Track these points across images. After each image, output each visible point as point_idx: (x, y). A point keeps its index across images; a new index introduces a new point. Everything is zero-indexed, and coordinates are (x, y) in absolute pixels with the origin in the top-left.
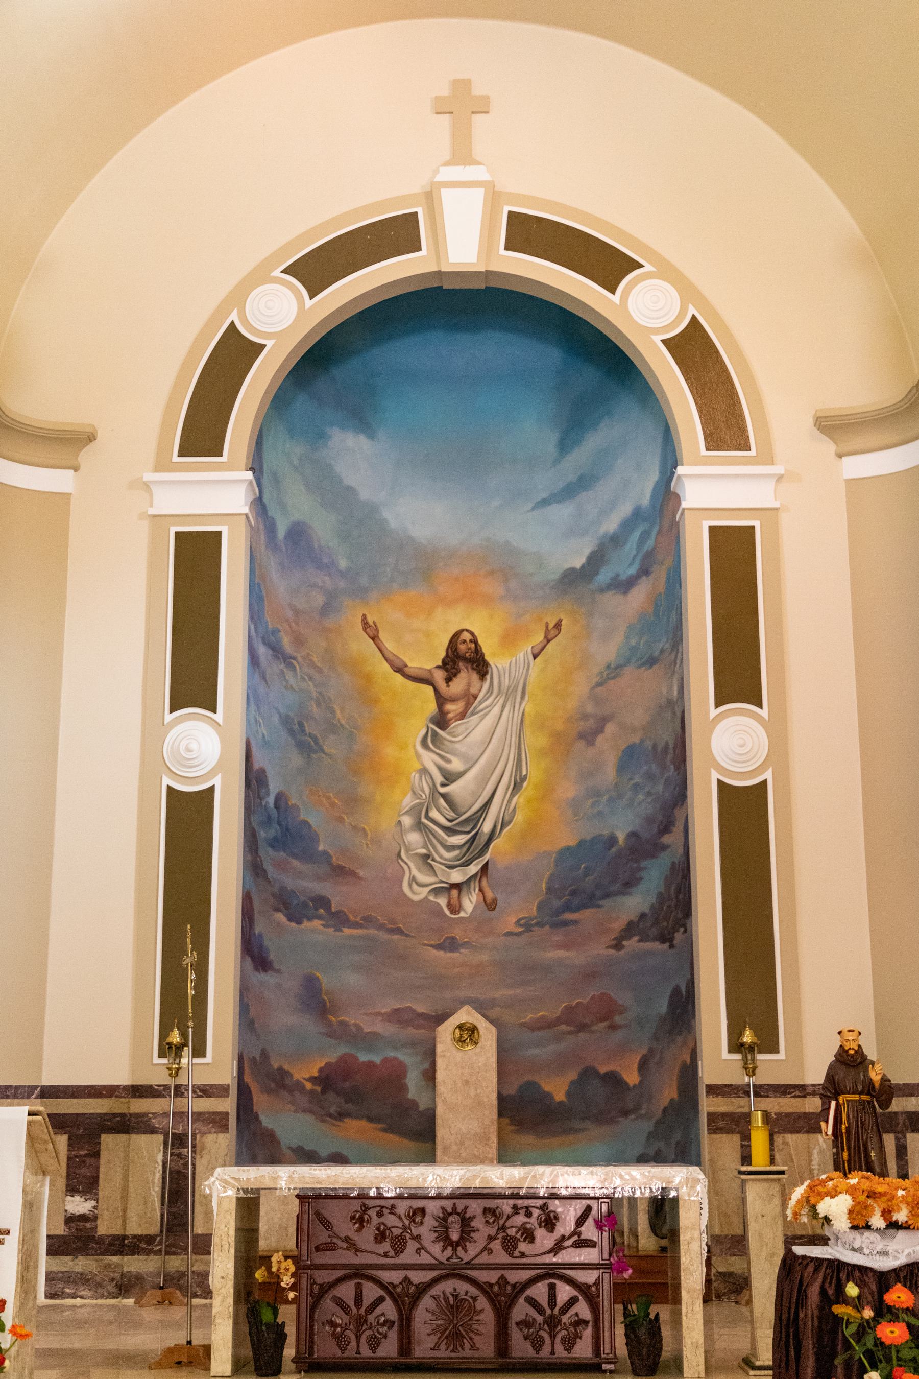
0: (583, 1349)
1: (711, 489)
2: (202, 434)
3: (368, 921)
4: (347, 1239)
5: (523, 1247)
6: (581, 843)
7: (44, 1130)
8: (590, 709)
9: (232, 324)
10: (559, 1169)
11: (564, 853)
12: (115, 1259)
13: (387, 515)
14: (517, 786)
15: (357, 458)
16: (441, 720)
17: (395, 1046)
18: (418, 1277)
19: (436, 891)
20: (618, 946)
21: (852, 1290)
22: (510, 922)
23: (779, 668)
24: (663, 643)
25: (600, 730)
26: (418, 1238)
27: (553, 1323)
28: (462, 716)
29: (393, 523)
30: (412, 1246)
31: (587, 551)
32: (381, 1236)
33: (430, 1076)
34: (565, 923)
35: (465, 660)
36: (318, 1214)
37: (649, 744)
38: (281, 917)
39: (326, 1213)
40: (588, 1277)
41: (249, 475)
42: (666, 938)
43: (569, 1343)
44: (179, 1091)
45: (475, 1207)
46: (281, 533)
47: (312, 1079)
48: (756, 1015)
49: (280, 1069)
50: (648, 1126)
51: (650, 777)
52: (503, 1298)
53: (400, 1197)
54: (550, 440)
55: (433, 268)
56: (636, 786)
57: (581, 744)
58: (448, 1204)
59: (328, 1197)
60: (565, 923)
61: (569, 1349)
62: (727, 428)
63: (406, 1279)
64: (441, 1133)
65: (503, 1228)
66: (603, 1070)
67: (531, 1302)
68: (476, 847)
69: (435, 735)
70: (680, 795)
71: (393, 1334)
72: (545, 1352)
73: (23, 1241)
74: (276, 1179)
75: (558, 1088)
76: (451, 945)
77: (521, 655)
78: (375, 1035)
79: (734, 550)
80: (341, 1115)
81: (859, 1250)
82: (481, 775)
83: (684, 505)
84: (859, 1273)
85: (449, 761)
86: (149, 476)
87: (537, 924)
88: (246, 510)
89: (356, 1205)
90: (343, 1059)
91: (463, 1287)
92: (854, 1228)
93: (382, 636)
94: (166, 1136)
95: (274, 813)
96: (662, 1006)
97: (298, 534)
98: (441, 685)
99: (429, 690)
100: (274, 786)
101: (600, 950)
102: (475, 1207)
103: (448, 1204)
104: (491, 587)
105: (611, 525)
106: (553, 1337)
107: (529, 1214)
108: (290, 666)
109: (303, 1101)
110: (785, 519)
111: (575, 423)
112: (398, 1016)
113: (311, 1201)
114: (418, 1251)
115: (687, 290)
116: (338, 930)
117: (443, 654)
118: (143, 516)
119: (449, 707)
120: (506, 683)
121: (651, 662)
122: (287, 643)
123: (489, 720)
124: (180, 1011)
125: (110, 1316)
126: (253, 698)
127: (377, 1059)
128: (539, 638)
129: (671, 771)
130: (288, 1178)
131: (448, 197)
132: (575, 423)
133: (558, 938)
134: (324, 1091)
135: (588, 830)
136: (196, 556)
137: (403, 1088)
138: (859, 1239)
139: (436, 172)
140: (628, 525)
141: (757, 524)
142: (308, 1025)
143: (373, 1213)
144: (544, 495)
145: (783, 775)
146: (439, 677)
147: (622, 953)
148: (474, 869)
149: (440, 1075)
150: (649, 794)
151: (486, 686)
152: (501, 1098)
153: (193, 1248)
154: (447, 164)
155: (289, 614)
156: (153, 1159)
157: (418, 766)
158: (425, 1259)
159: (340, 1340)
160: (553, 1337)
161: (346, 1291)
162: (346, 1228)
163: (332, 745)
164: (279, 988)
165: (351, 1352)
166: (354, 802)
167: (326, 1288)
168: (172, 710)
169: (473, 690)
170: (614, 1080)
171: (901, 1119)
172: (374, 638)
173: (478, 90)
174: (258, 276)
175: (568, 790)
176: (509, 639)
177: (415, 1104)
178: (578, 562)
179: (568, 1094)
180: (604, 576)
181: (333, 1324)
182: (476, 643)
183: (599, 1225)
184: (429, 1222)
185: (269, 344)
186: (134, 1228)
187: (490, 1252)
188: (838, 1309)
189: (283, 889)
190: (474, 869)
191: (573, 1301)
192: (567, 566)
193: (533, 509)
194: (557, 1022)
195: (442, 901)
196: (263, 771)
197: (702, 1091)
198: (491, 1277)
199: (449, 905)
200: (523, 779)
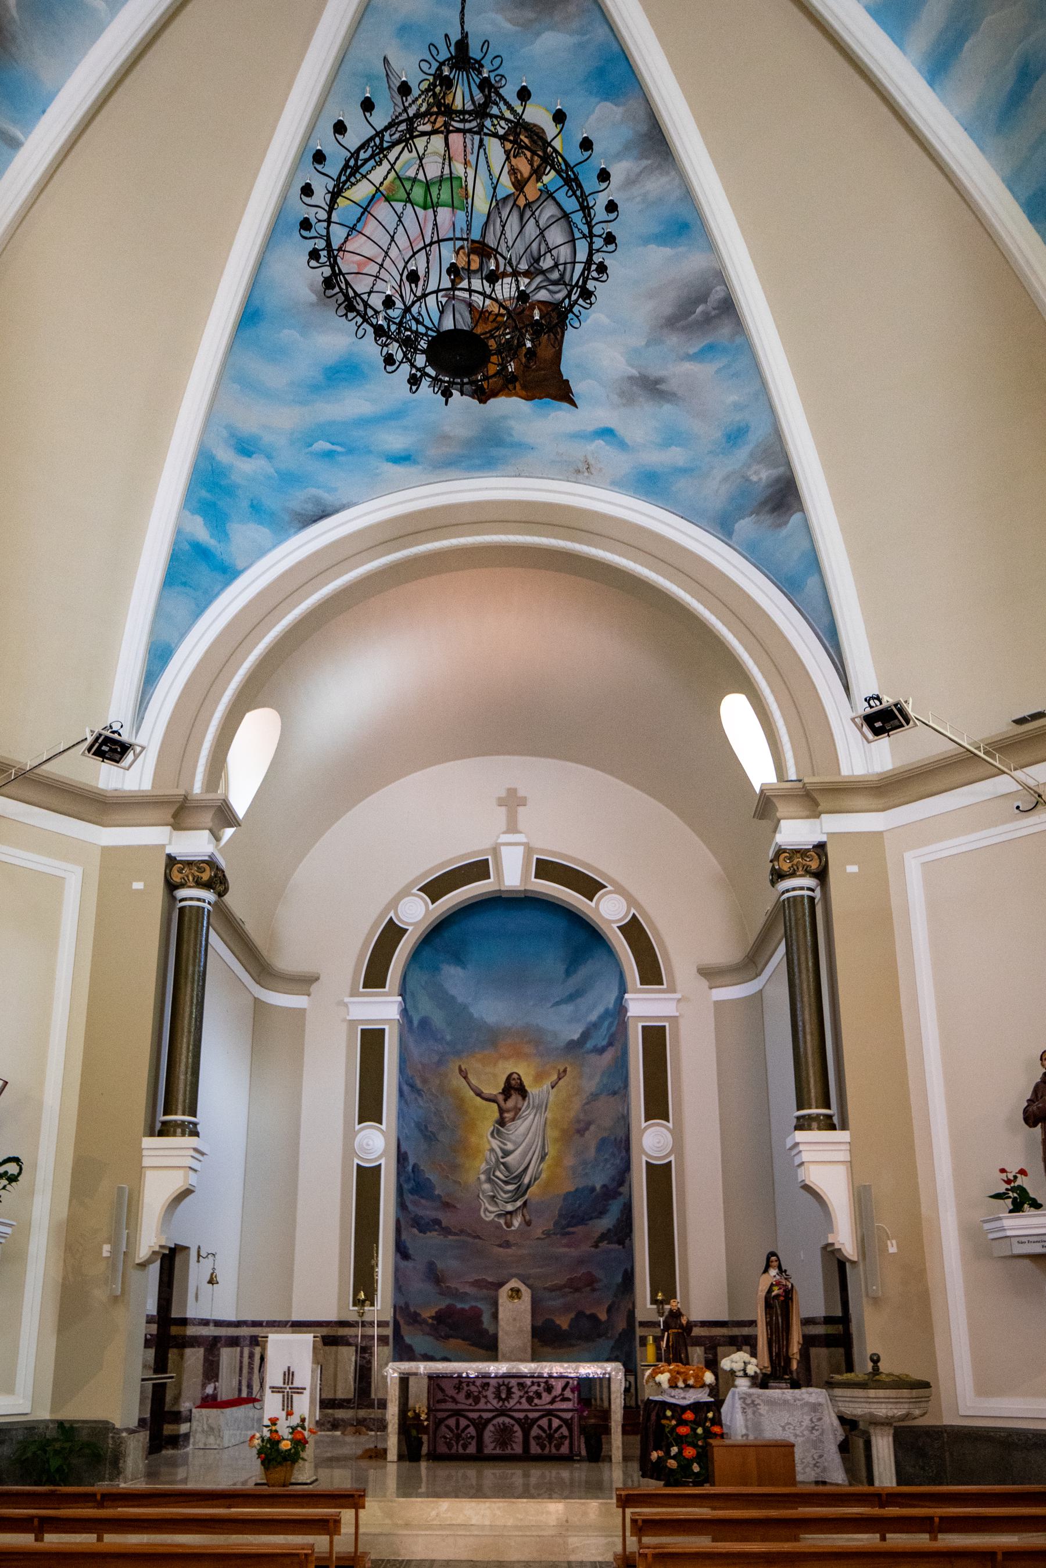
0: (565, 1449)
1: (643, 1006)
2: (375, 977)
3: (462, 1231)
4: (452, 1397)
5: (536, 1401)
6: (577, 1190)
7: (320, 1345)
8: (582, 1117)
9: (391, 918)
10: (553, 1364)
12: (330, 1411)
13: (472, 1010)
14: (543, 1158)
15: (455, 979)
16: (502, 1122)
17: (476, 1299)
18: (486, 1415)
19: (499, 1216)
20: (596, 1246)
21: (669, 1413)
22: (538, 1232)
23: (679, 1104)
24: (620, 1084)
25: (587, 1129)
26: (486, 1397)
27: (550, 1437)
28: (513, 1119)
29: (476, 1015)
30: (483, 1400)
31: (580, 1031)
32: (468, 1395)
33: (495, 1316)
34: (569, 1233)
35: (516, 1090)
36: (438, 1385)
37: (613, 1138)
38: (415, 1231)
39: (443, 1385)
40: (568, 1416)
41: (400, 999)
42: (621, 1242)
43: (558, 1447)
44: (364, 1324)
45: (513, 1382)
46: (416, 1023)
47: (432, 1318)
49: (415, 1312)
50: (612, 1343)
51: (613, 1155)
52: (527, 1425)
53: (477, 1377)
54: (561, 968)
55: (497, 888)
56: (606, 1159)
57: (577, 1136)
58: (500, 1381)
59: (443, 1377)
60: (569, 1233)
61: (558, 1450)
62: (651, 973)
63: (480, 1417)
64: (501, 1346)
65: (527, 1392)
66: (588, 1312)
67: (540, 1427)
68: (520, 1192)
69: (498, 1130)
70: (626, 1168)
71: (474, 1443)
72: (546, 1451)
73: (311, 1394)
74: (418, 1368)
75: (564, 1322)
76: (507, 1245)
77: (545, 1087)
78: (466, 1293)
79: (655, 1038)
80: (447, 1337)
81: (673, 1397)
83: (629, 1014)
84: (673, 1407)
85: (505, 1144)
86: (347, 999)
87: (554, 1234)
88: (398, 1017)
89: (456, 1381)
90: (449, 1307)
91: (507, 1420)
92: (671, 1387)
93: (470, 1076)
94: (357, 1347)
95: (412, 1175)
96: (619, 1279)
97: (425, 1023)
98: (502, 1103)
99: (495, 1106)
100: (412, 1160)
101: (586, 1248)
102: (513, 1382)
103: (500, 1381)
104: (528, 1049)
105: (593, 1017)
106: (550, 1443)
107: (539, 1385)
108: (420, 1095)
109: (427, 1329)
110: (681, 1021)
111: (574, 960)
112: (478, 1284)
113: (435, 1380)
114: (486, 1403)
115: (631, 901)
116: (445, 1237)
117: (502, 1086)
118: (344, 1020)
119: (506, 1115)
120: (537, 1101)
121: (614, 1093)
122: (419, 1084)
124: (364, 1280)
125: (328, 1440)
126: (401, 1115)
127: (467, 1306)
128: (555, 1077)
129: (624, 1154)
130: (423, 1367)
131: (504, 850)
132: (574, 960)
133: (564, 1241)
134: (438, 1324)
135: (581, 1183)
136: (372, 1041)
137: (481, 1322)
138: (673, 1392)
139: (498, 837)
140: (602, 1018)
141: (667, 1024)
142: (429, 1288)
143: (464, 1385)
144: (557, 999)
145: (680, 1156)
146: (501, 1098)
147: (597, 1250)
149: (501, 1316)
150: (613, 1164)
151: (526, 1104)
152: (533, 1328)
153: (803, 1117)
154: (504, 833)
155: (420, 1066)
156: (350, 1360)
157: (488, 1147)
158: (489, 1407)
159: (449, 1446)
160: (550, 1443)
161: (452, 1422)
162: (451, 1392)
163: (442, 1136)
164: (415, 1268)
165: (453, 1451)
166: (455, 1167)
168: (360, 1123)
169: (519, 1106)
170: (593, 1318)
171: (740, 1339)
172: (465, 1078)
173: (521, 793)
174: (405, 893)
175: (569, 1161)
176: (539, 1078)
177: (487, 1331)
178: (576, 1036)
179: (570, 1326)
180: (589, 1045)
181: (446, 1438)
182: (520, 1079)
183: (573, 1391)
184: (491, 1389)
185: (410, 928)
186: (340, 1395)
187: (520, 1403)
188: (664, 1422)
189: (416, 1215)
190: (519, 1203)
191: (560, 1427)
193: (553, 1006)
194: (564, 1286)
195: (502, 1221)
196: (406, 1153)
197: (637, 1324)
198: (521, 1415)
199: (506, 1223)
200: (546, 1154)
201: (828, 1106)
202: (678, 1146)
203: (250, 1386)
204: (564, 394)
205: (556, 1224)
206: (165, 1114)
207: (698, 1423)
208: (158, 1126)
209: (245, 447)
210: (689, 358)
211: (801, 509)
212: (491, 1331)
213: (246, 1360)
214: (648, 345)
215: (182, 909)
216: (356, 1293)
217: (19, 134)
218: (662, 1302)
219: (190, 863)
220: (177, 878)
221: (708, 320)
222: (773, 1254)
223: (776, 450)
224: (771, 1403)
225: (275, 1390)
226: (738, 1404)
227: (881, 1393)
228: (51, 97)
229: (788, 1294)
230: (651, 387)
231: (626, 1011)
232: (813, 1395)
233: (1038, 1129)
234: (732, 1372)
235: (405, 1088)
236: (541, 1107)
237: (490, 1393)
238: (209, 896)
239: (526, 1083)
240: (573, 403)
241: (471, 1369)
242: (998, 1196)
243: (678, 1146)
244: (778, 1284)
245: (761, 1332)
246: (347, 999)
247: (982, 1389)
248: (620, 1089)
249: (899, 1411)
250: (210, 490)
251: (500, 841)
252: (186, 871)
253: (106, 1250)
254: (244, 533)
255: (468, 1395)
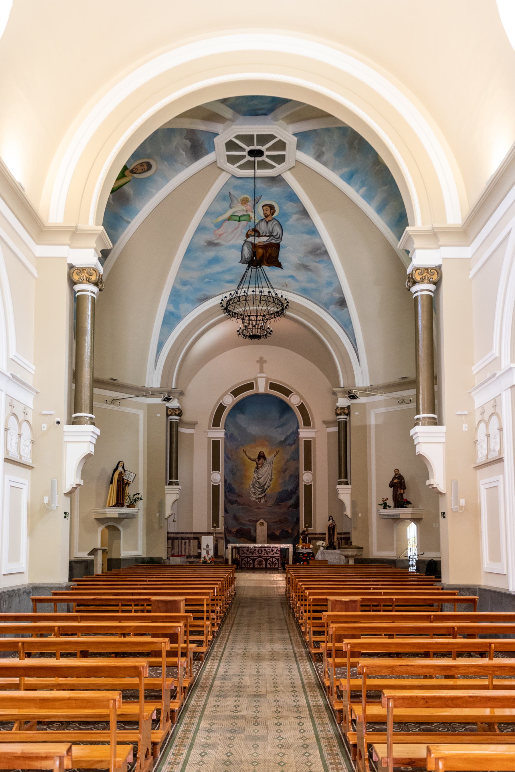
1: (304, 433)
2: (216, 423)
3: (244, 504)
8: (284, 467)
11: (279, 492)
13: (247, 430)
14: (271, 480)
15: (242, 419)
16: (257, 468)
18: (255, 558)
19: (256, 499)
22: (270, 504)
25: (286, 471)
28: (261, 467)
33: (255, 531)
34: (279, 505)
40: (277, 558)
43: (275, 566)
45: (263, 549)
48: (309, 522)
50: (293, 539)
52: (266, 560)
60: (279, 505)
62: (307, 423)
68: (264, 491)
70: (298, 485)
75: (278, 533)
79: (308, 444)
80: (240, 537)
82: (264, 477)
86: (207, 430)
96: (295, 520)
97: (232, 435)
99: (255, 462)
100: (228, 482)
102: (263, 549)
105: (289, 433)
110: (317, 439)
112: (249, 521)
115: (301, 397)
118: (206, 437)
123: (266, 468)
128: (275, 453)
136: (216, 444)
137: (251, 533)
145: (315, 483)
146: (257, 460)
148: (263, 495)
152: (268, 534)
162: (246, 551)
167: (244, 559)
170: (287, 531)
174: (225, 394)
175: (280, 481)
176: (270, 453)
178: (283, 440)
180: (287, 443)
190: (263, 495)
192: (280, 440)
194: (278, 522)
195: (258, 501)
198: (265, 558)
201: (347, 478)
202: (314, 479)
203: (181, 552)
204: (279, 265)
205: (275, 501)
206: (170, 479)
207: (307, 557)
208: (168, 482)
209: (184, 283)
210: (315, 262)
211: (347, 307)
212: (254, 535)
213: (180, 544)
214: (304, 256)
215: (171, 422)
216: (213, 524)
217: (130, 220)
218: (308, 527)
219: (173, 409)
220: (169, 413)
221: (320, 254)
222: (331, 516)
223: (340, 290)
224: (328, 553)
225: (204, 549)
226: (320, 553)
227: (350, 550)
228: (139, 211)
229: (334, 526)
230: (305, 267)
231: (299, 435)
232: (338, 551)
233: (392, 488)
234: (319, 546)
235: (226, 458)
236: (271, 463)
237: (256, 552)
238: (178, 418)
239: (266, 455)
240: (282, 268)
241: (251, 546)
242: (381, 505)
243: (314, 479)
244: (332, 524)
245: (327, 536)
246: (207, 430)
247: (379, 550)
248: (296, 459)
249: (355, 554)
250: (176, 297)
251: (257, 376)
252: (172, 411)
253: (158, 515)
254: (184, 306)
255: (250, 552)
